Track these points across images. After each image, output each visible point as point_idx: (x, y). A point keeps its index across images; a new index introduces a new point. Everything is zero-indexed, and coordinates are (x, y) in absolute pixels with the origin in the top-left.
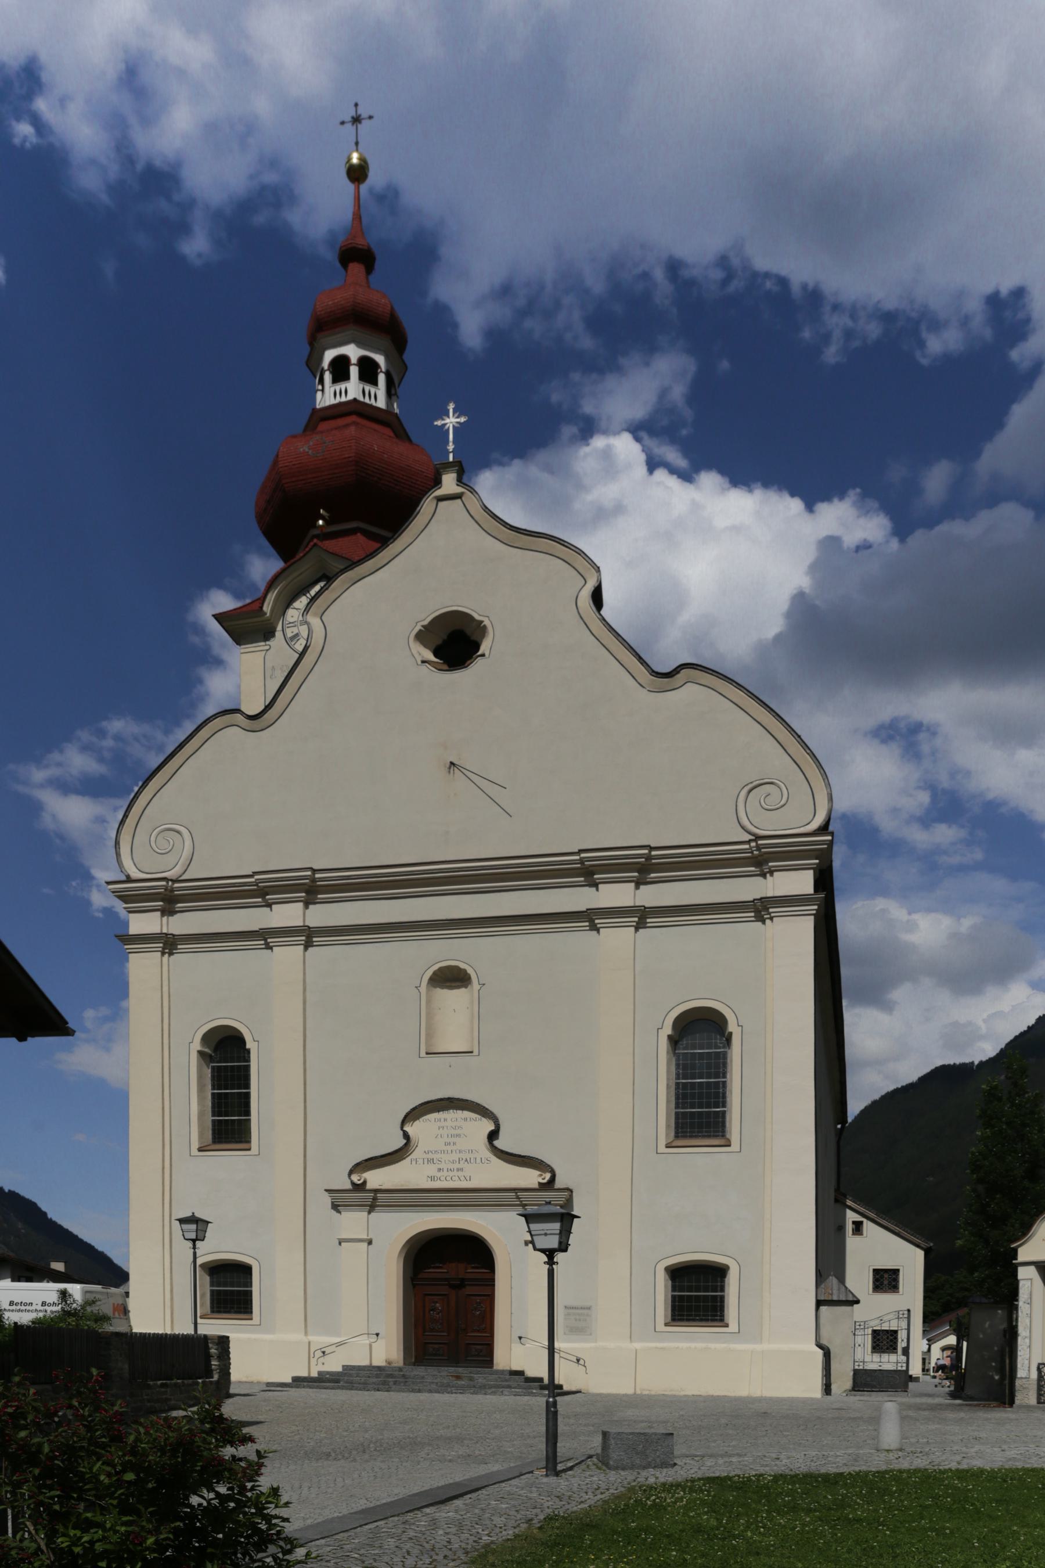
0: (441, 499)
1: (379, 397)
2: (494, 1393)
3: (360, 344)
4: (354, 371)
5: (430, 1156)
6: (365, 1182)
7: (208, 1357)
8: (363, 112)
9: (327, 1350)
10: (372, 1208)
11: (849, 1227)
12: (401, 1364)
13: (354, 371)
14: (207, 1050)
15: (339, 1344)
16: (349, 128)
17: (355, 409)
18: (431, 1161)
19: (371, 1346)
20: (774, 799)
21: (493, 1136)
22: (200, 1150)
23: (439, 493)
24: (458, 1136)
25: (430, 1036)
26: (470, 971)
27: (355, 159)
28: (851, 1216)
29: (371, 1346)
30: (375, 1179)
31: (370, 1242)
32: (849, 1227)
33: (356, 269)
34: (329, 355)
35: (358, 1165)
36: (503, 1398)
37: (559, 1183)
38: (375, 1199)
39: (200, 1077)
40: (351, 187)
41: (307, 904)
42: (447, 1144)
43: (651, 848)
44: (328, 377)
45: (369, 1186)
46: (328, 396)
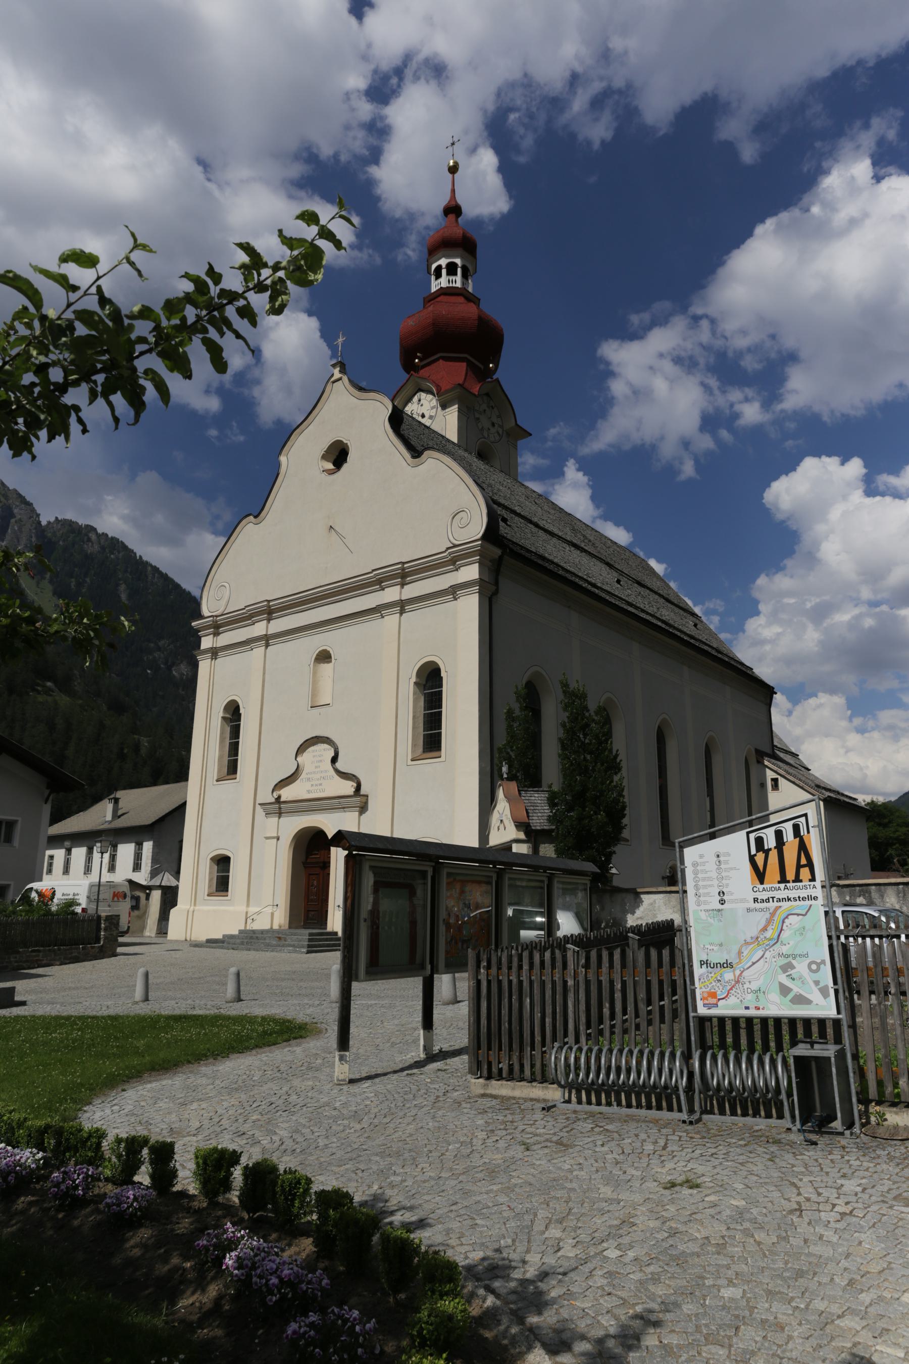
0: (334, 382)
1: (458, 281)
2: (272, 951)
3: (447, 257)
4: (444, 272)
5: (309, 776)
6: (279, 797)
7: (99, 929)
8: (455, 139)
9: (255, 917)
10: (280, 814)
11: (769, 784)
12: (287, 927)
13: (444, 272)
14: (228, 716)
15: (259, 913)
16: (450, 148)
17: (443, 292)
18: (309, 779)
19: (272, 914)
20: (464, 522)
21: (334, 760)
22: (217, 781)
23: (333, 379)
24: (321, 761)
25: (314, 693)
26: (331, 652)
27: (451, 163)
28: (770, 775)
29: (272, 914)
30: (287, 793)
31: (278, 839)
32: (769, 784)
33: (452, 217)
34: (434, 266)
35: (276, 785)
36: (283, 955)
37: (363, 791)
38: (280, 808)
39: (222, 733)
40: (451, 176)
41: (269, 620)
42: (316, 767)
43: (404, 563)
44: (433, 278)
45: (283, 799)
46: (435, 286)
